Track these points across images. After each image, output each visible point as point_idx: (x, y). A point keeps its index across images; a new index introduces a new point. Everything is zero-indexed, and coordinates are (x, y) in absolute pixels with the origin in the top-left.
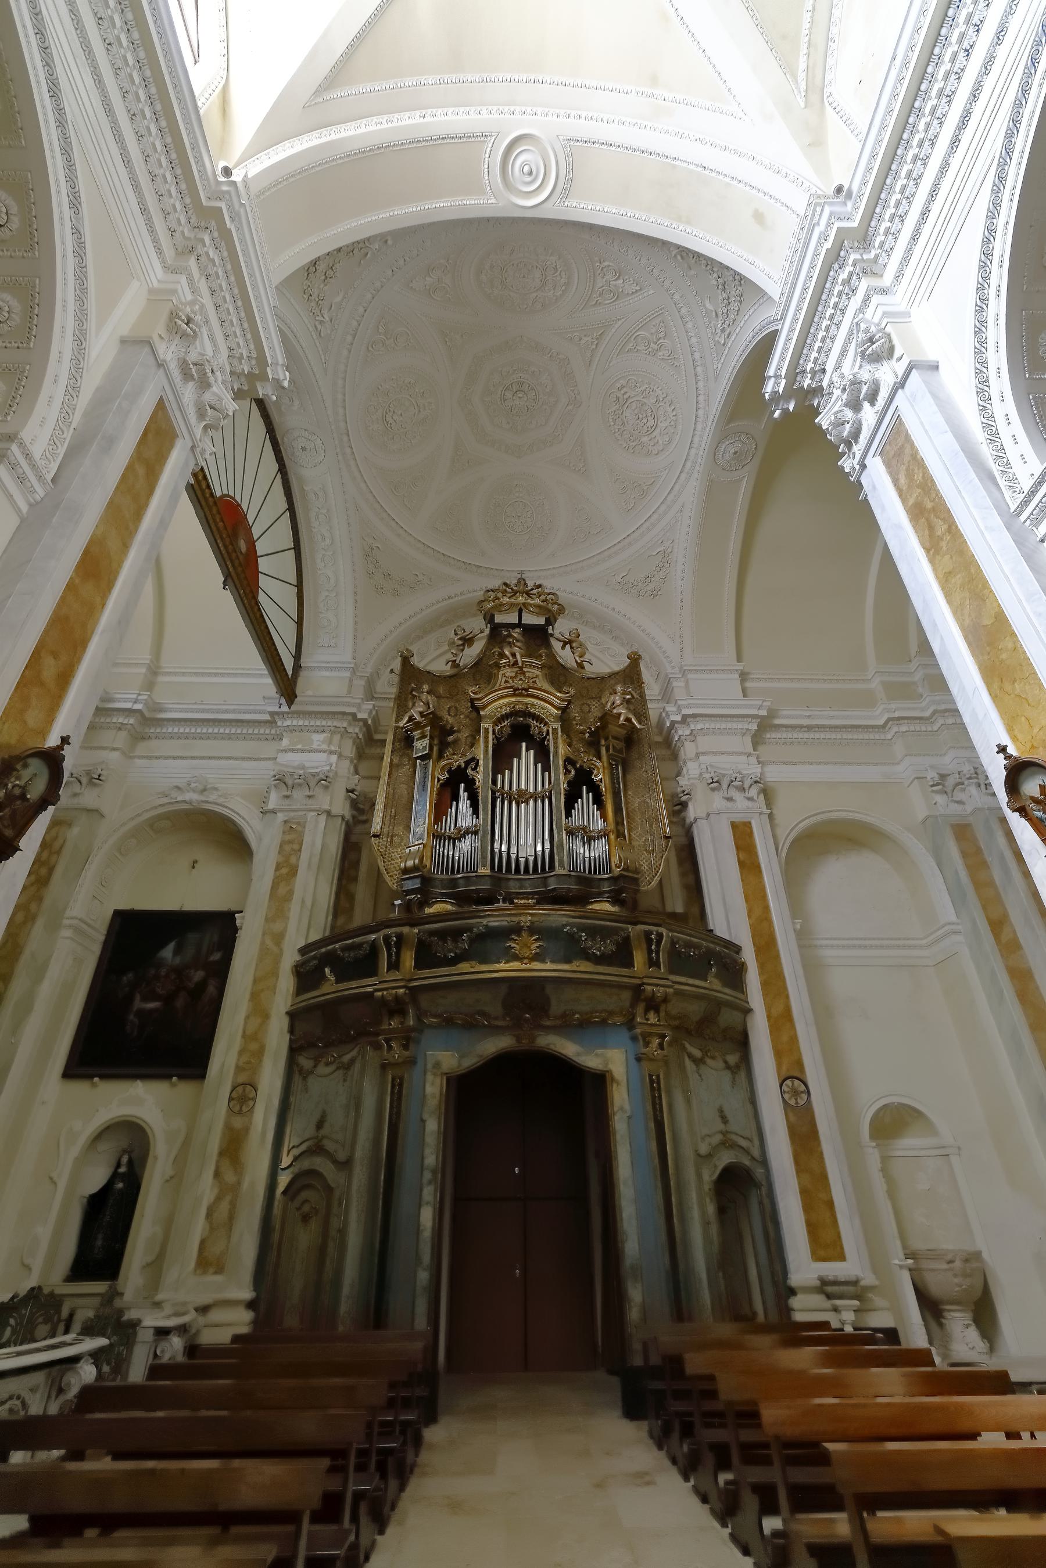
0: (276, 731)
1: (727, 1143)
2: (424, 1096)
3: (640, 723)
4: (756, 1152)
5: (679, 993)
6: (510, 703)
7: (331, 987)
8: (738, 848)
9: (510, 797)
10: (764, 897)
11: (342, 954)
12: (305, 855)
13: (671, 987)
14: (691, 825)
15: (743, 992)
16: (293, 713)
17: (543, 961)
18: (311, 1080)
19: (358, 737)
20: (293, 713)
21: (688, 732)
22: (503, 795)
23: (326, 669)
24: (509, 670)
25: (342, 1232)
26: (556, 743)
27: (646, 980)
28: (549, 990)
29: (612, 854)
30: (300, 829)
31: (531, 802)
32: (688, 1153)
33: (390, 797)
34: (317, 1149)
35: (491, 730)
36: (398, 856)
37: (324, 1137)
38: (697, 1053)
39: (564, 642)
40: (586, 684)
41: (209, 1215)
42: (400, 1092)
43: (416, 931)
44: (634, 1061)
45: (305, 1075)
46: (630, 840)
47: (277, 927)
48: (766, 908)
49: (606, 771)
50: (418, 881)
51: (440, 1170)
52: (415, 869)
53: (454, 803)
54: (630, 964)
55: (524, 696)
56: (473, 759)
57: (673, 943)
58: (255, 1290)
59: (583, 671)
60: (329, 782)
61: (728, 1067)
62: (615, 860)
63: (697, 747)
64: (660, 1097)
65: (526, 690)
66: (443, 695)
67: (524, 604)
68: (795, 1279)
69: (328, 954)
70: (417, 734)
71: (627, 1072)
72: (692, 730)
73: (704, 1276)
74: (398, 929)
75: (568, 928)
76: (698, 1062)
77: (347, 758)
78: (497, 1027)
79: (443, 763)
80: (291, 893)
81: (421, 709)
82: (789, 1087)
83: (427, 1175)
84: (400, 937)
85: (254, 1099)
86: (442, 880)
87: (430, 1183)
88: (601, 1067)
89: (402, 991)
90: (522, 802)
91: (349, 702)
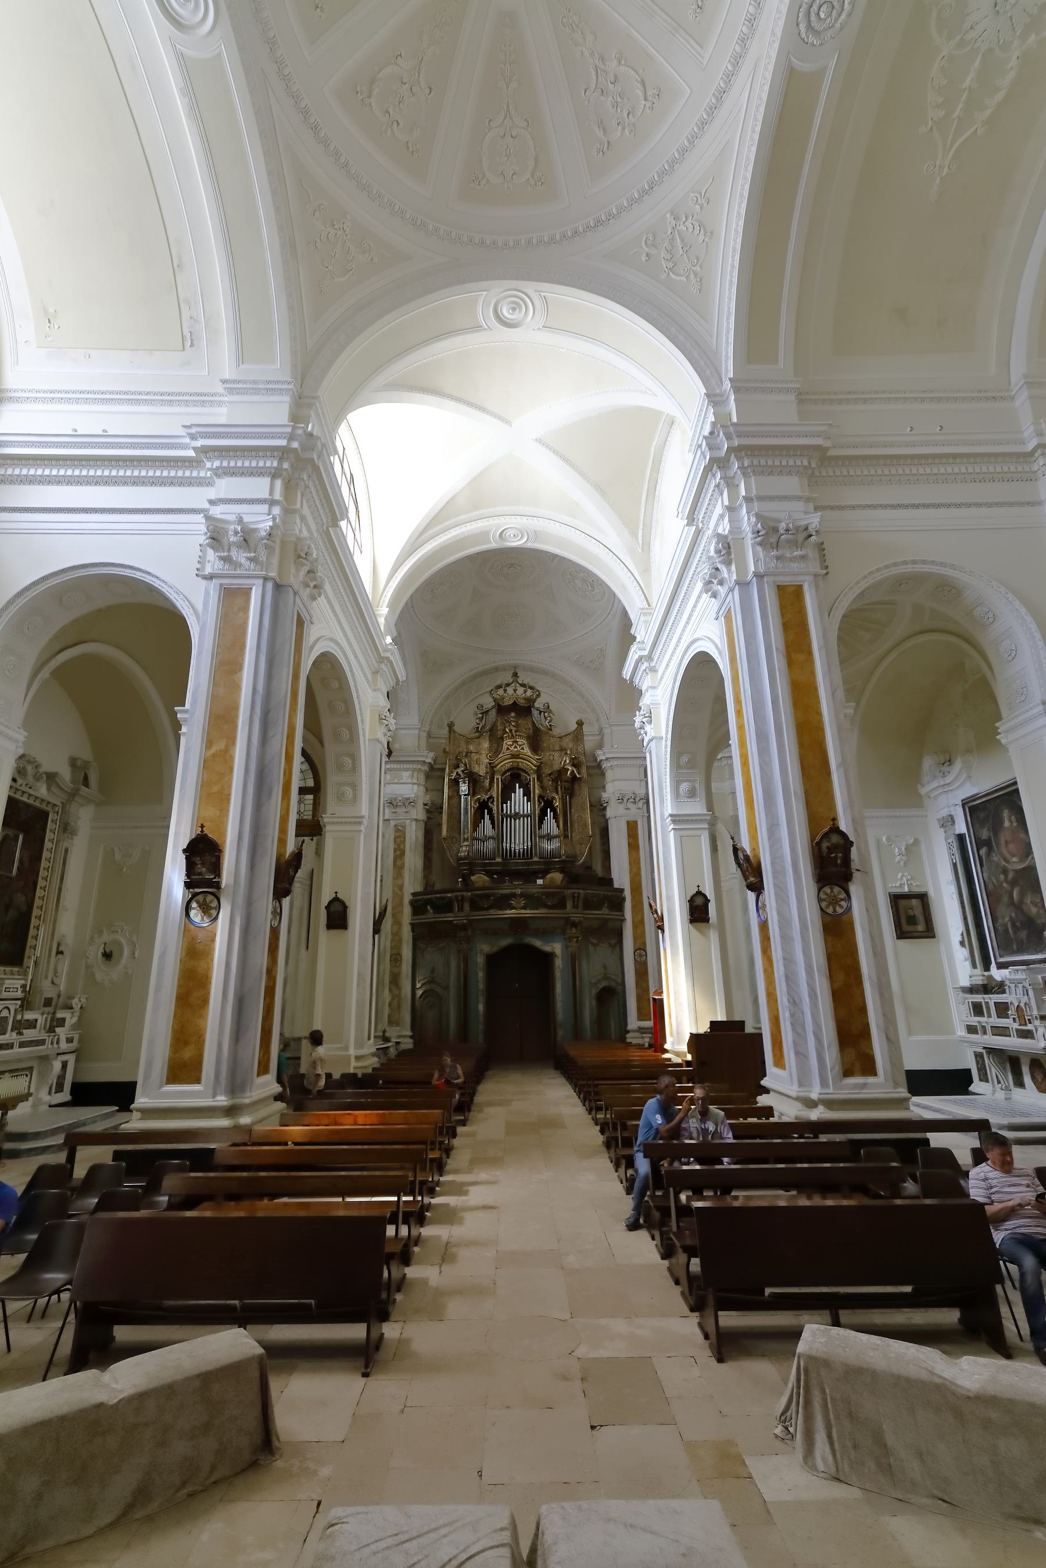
1: (606, 977)
3: (579, 774)
7: (430, 916)
8: (629, 836)
10: (639, 863)
16: (391, 761)
17: (526, 909)
20: (391, 761)
23: (404, 729)
34: (431, 981)
41: (390, 1005)
43: (469, 894)
46: (571, 837)
47: (399, 882)
48: (639, 869)
62: (563, 852)
68: (629, 1027)
73: (588, 1026)
74: (463, 893)
76: (594, 945)
80: (403, 864)
82: (826, 894)
84: (462, 896)
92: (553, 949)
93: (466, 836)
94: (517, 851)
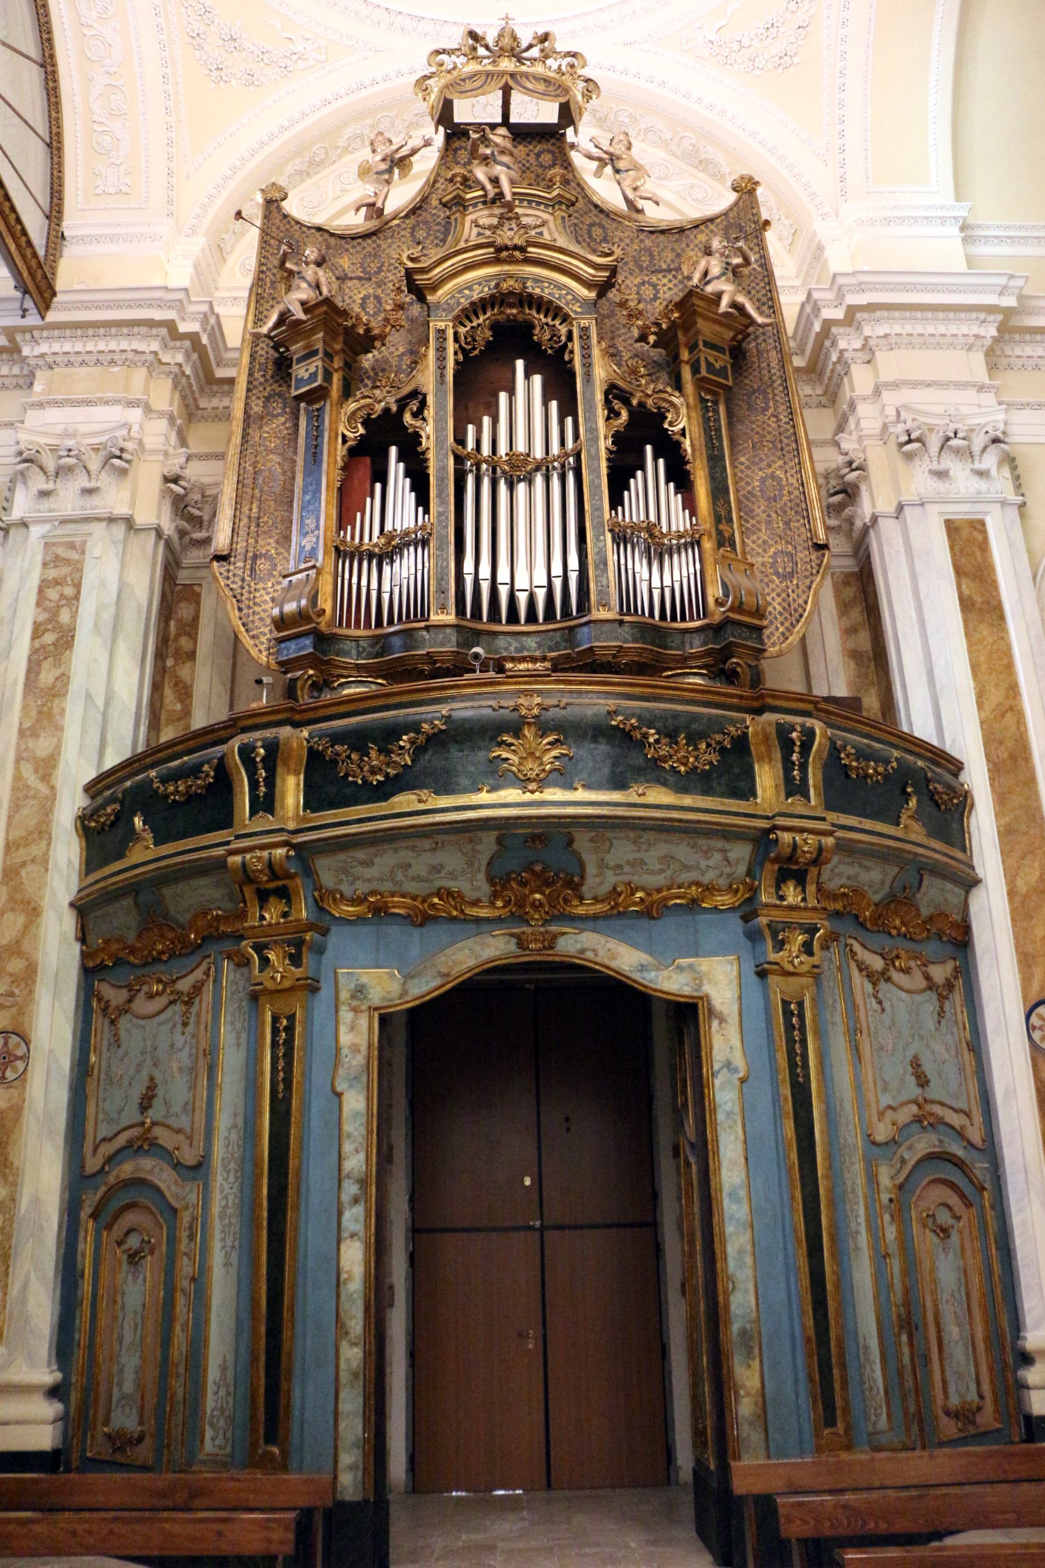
0: (22, 369)
2: (338, 1049)
4: (975, 1135)
5: (845, 848)
6: (488, 279)
8: (959, 572)
9: (494, 471)
11: (162, 788)
12: (87, 607)
13: (830, 833)
14: (865, 531)
15: (964, 849)
18: (124, 1022)
19: (183, 373)
21: (858, 344)
22: (478, 465)
24: (486, 212)
25: (200, 1281)
26: (587, 356)
27: (781, 821)
28: (583, 842)
29: (708, 579)
30: (74, 556)
31: (539, 480)
32: (852, 1136)
33: (249, 481)
35: (450, 333)
36: (267, 598)
37: (154, 1124)
38: (877, 963)
39: (600, 159)
40: (648, 243)
42: (289, 1043)
43: (305, 734)
44: (755, 977)
45: (113, 1015)
46: (744, 553)
47: (42, 746)
48: (1013, 689)
49: (693, 414)
50: (308, 642)
51: (374, 1180)
52: (302, 616)
53: (378, 486)
54: (748, 792)
55: (517, 262)
56: (415, 394)
57: (835, 750)
58: (60, 1369)
59: (640, 217)
60: (127, 461)
61: (931, 986)
62: (714, 591)
63: (876, 372)
64: (804, 1042)
65: (522, 249)
66: (350, 275)
67: (512, 75)
69: (139, 788)
70: (297, 348)
71: (740, 998)
72: (866, 339)
73: (874, 1343)
74: (268, 733)
75: (620, 718)
77: (161, 414)
78: (478, 920)
79: (353, 406)
80: (64, 679)
81: (303, 296)
83: (351, 1189)
85: (25, 1058)
86: (356, 640)
87: (356, 1201)
88: (687, 991)
89: (280, 852)
90: (520, 481)
91: (160, 299)
92: (699, 979)
93: (308, 543)
94: (522, 598)
